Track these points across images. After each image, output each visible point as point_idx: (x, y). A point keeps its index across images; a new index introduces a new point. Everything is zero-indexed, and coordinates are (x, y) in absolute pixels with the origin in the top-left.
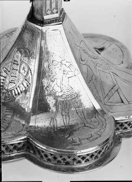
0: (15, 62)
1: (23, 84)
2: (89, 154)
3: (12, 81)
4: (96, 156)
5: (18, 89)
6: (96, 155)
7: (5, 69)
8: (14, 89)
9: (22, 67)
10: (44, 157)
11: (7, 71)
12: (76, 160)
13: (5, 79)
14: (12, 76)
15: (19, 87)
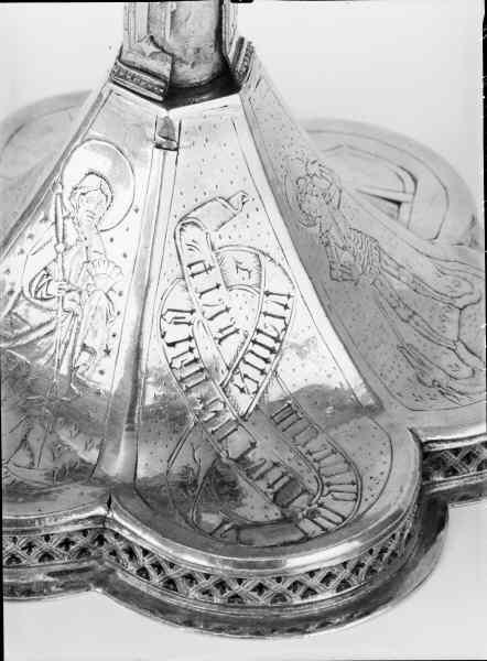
0: (195, 269)
1: (266, 314)
2: (318, 570)
3: (221, 331)
4: (343, 581)
5: (260, 338)
6: (344, 574)
7: (169, 316)
8: (250, 348)
9: (230, 265)
10: (152, 572)
11: (180, 315)
12: (267, 588)
13: (192, 344)
14: (211, 319)
15: (259, 331)
